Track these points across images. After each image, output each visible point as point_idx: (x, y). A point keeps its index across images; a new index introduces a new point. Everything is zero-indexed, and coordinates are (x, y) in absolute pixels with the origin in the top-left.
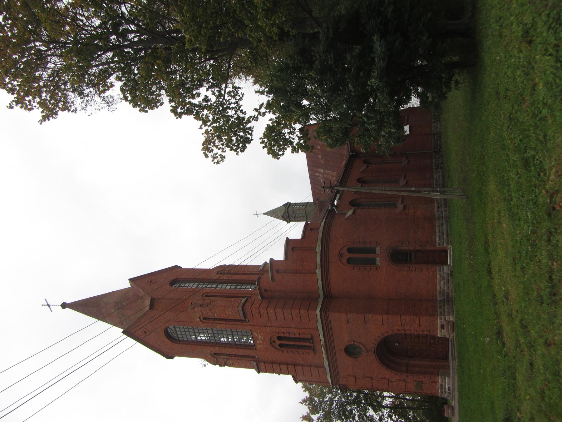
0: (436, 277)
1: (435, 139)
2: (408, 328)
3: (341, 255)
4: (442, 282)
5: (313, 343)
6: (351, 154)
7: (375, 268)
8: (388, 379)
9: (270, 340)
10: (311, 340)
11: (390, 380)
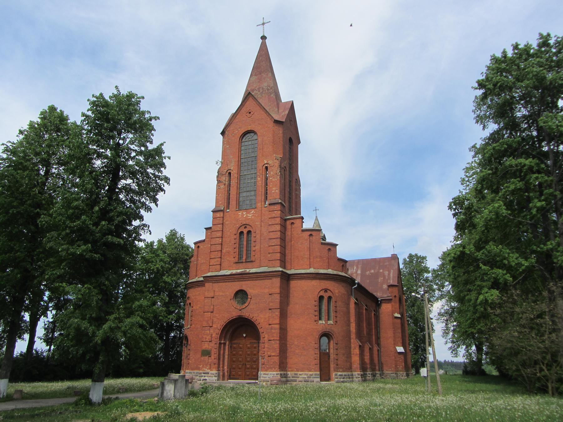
0: (310, 371)
1: (392, 374)
2: (266, 346)
3: (327, 291)
4: (305, 376)
5: (246, 262)
6: (379, 299)
7: (316, 320)
8: (212, 327)
9: (248, 225)
10: (249, 261)
11: (211, 328)
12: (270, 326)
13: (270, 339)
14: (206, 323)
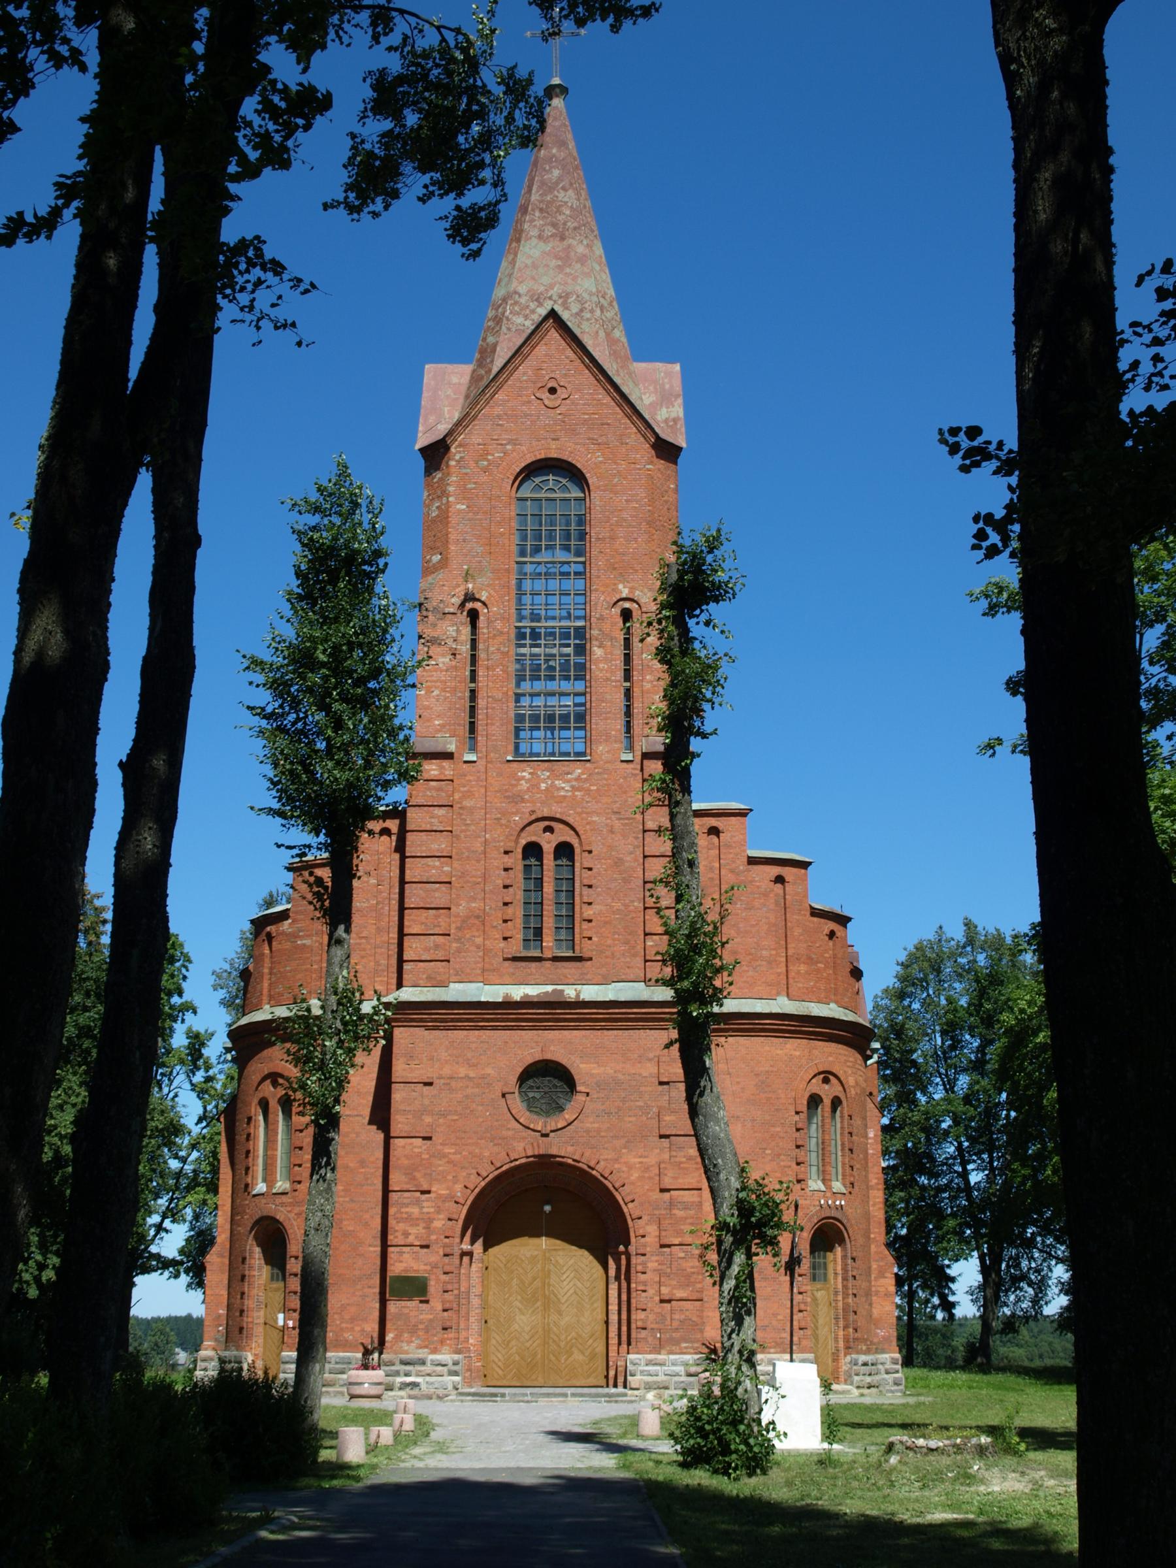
2: (652, 1265)
8: (429, 1192)
12: (667, 1195)
13: (666, 1241)
14: (403, 1178)
